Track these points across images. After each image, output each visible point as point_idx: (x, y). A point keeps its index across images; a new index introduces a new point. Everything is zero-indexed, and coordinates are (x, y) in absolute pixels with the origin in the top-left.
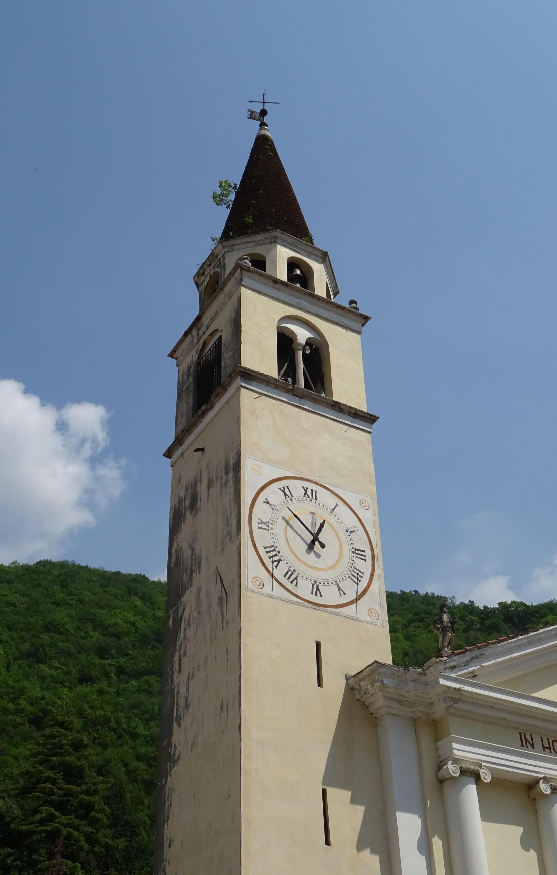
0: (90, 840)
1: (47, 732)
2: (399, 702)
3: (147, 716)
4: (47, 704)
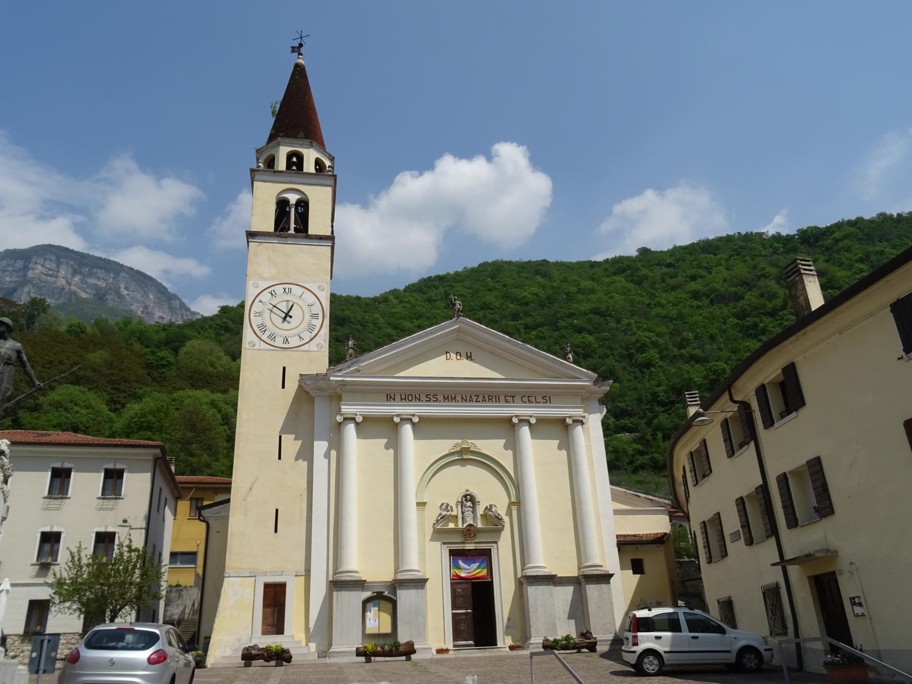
2: (320, 390)
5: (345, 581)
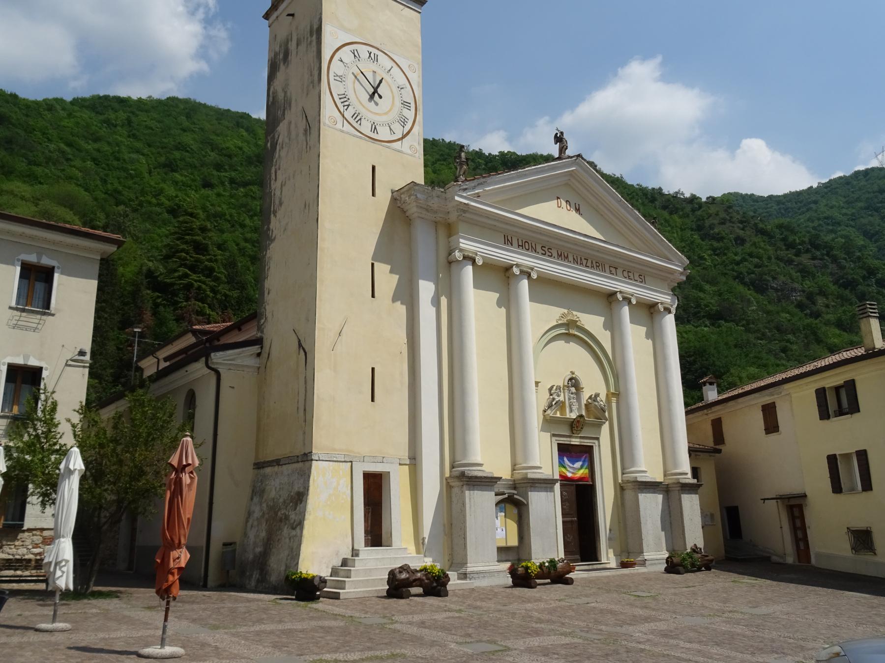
0: (213, 290)
1: (181, 219)
2: (427, 210)
3: (251, 213)
4: (180, 201)
5: (476, 477)
